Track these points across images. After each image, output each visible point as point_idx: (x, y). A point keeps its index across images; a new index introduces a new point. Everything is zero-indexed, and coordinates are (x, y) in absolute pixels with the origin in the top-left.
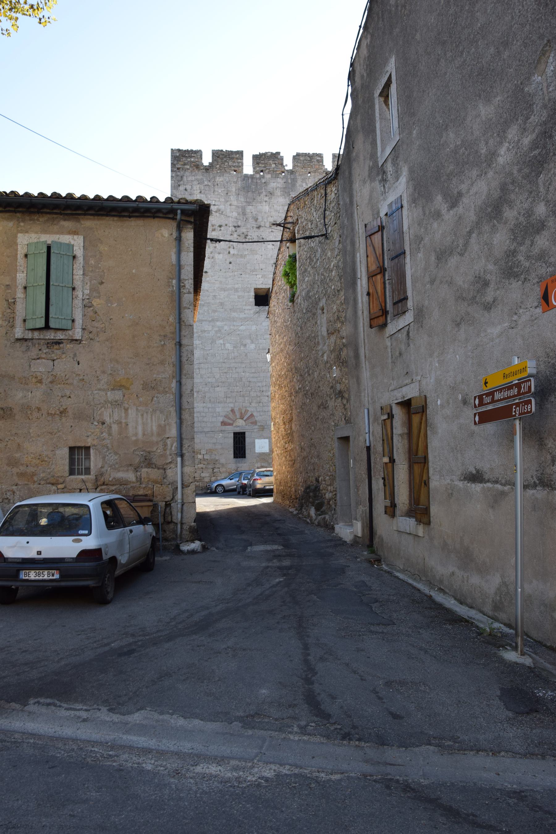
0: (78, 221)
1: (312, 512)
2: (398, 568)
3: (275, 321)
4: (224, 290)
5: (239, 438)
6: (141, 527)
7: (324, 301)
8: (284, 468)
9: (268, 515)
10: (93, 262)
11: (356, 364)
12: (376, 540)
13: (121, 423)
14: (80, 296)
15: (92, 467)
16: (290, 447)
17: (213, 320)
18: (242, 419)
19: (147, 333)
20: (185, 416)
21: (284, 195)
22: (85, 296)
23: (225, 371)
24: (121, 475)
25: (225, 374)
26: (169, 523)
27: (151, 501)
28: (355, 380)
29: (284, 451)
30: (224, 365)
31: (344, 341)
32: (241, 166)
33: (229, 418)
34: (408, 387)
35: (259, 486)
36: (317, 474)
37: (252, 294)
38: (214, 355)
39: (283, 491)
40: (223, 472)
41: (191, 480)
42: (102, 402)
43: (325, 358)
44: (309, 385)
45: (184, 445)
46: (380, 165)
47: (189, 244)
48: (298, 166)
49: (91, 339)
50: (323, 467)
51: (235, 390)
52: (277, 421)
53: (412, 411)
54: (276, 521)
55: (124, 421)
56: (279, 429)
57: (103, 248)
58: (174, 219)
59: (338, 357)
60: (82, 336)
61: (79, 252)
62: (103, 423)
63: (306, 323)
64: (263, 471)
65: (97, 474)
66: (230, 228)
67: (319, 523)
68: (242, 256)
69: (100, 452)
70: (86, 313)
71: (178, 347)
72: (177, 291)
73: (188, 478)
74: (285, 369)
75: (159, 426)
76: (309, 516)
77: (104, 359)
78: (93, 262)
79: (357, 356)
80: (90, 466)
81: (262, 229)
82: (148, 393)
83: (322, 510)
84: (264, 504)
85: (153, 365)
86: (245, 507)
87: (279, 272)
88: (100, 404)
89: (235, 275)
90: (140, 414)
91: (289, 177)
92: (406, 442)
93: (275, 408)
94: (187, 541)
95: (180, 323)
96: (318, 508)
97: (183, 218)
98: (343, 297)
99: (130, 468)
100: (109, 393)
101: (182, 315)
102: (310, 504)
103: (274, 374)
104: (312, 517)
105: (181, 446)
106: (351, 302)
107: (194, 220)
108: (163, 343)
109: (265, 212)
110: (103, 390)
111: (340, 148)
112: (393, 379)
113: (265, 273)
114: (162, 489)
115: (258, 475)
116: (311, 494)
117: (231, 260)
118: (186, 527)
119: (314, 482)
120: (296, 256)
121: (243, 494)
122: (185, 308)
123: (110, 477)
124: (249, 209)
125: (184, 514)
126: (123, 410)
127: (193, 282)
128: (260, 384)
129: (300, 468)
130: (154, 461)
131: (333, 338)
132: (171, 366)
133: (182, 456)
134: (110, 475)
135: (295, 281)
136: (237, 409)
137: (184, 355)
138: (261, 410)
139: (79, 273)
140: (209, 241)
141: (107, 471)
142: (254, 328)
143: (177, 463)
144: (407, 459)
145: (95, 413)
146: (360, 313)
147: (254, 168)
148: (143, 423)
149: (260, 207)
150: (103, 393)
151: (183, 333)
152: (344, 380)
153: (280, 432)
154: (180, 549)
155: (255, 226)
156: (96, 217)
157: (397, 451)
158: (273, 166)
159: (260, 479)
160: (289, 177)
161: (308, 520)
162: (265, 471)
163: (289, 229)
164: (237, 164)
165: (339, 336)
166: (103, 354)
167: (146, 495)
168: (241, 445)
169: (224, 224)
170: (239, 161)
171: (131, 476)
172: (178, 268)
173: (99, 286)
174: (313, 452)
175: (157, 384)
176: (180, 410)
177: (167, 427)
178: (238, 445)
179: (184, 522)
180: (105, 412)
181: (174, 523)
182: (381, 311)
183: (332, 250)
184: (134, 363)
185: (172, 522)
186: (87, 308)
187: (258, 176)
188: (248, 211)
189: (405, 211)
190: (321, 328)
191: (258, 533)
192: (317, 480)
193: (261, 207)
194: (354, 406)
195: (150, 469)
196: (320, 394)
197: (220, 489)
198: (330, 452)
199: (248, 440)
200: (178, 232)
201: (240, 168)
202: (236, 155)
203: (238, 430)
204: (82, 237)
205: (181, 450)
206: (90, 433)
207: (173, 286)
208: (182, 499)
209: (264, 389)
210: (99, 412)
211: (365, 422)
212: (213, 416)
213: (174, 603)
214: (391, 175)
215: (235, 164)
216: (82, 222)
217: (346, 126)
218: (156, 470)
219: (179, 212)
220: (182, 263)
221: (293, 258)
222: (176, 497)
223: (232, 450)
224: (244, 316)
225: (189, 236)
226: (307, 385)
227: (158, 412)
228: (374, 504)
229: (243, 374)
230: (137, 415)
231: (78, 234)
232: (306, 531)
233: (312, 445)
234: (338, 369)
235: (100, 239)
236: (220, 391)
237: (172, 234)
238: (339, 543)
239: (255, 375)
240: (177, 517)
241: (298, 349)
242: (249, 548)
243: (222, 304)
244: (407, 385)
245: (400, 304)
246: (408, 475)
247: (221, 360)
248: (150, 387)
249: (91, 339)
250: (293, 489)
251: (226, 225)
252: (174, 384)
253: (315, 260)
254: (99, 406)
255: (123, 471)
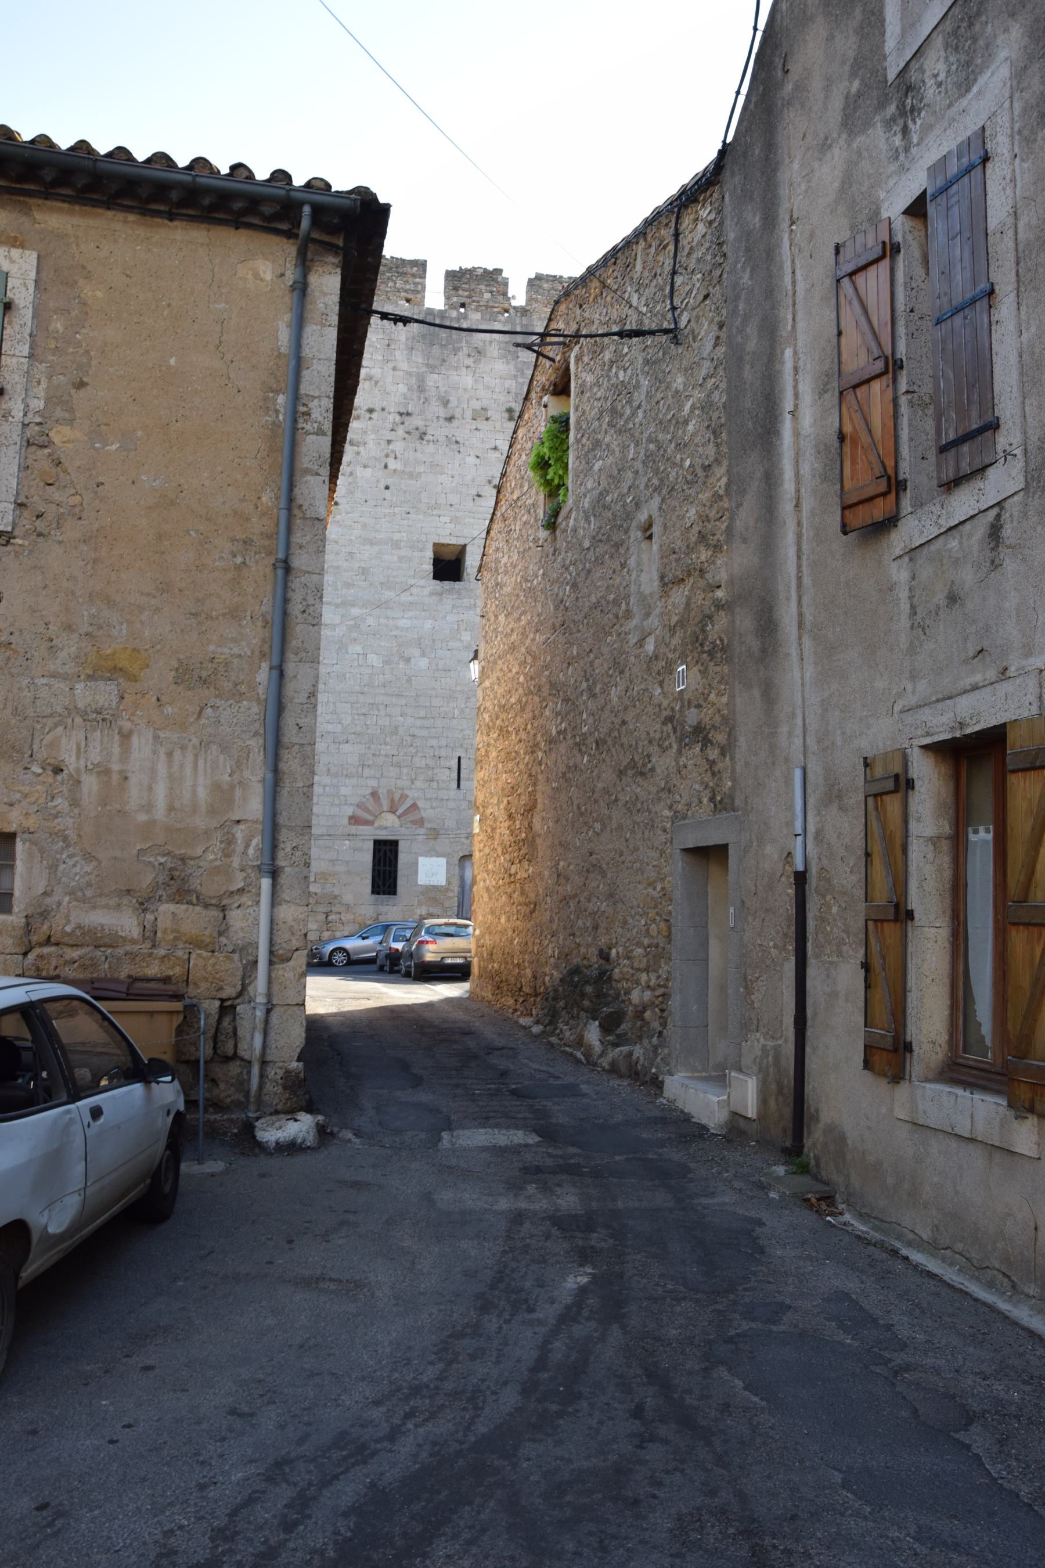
0: (26, 211)
1: (593, 1034)
2: (911, 1236)
3: (497, 584)
4: (372, 543)
5: (385, 852)
6: (137, 1088)
7: (656, 501)
8: (503, 920)
9: (467, 1032)
10: (59, 326)
11: (764, 651)
12: (815, 1139)
13: (107, 772)
14: (18, 414)
15: (17, 893)
16: (522, 872)
17: (344, 604)
18: (394, 813)
19: (197, 531)
20: (290, 763)
21: (505, 357)
22: (30, 415)
23: (363, 711)
24: (99, 918)
25: (362, 717)
26: (227, 1059)
27: (178, 997)
28: (756, 692)
29: (507, 880)
30: (361, 698)
31: (720, 594)
32: (420, 290)
33: (367, 810)
34: (985, 693)
35: (429, 957)
36: (603, 941)
37: (429, 554)
38: (342, 677)
39: (498, 973)
40: (349, 922)
41: (295, 943)
42: (59, 710)
43: (650, 647)
44: (591, 720)
45: (282, 845)
46: (891, 75)
47: (326, 306)
48: (537, 300)
49: (40, 535)
50: (625, 922)
51: (383, 752)
52: (488, 812)
53: (1011, 763)
54: (491, 1049)
55: (115, 767)
56: (494, 829)
57: (93, 292)
58: (290, 235)
59: (698, 640)
60: (14, 525)
61: (22, 294)
62: (58, 770)
63: (589, 572)
64: (440, 925)
65: (29, 912)
66: (391, 417)
67: (613, 1064)
68: (411, 476)
69: (42, 851)
70: (29, 462)
71: (280, 572)
72: (287, 426)
73: (287, 936)
74: (521, 691)
75: (216, 787)
76: (580, 1042)
77: (73, 593)
78: (59, 326)
79: (767, 625)
80: (13, 889)
81: (455, 423)
82: (189, 693)
83: (619, 1031)
84: (449, 1001)
85: (209, 617)
86: (407, 1006)
87: (514, 470)
88: (51, 716)
89: (394, 514)
90: (162, 751)
91: (518, 321)
92: (946, 860)
93: (485, 782)
94: (277, 1112)
95: (289, 509)
96: (610, 1025)
97: (316, 235)
98: (724, 480)
99: (125, 900)
100: (79, 687)
101: (296, 491)
102: (583, 1015)
103: (488, 704)
104: (590, 1047)
105: (274, 846)
106: (755, 487)
107: (345, 244)
108: (239, 560)
109: (465, 390)
110: (65, 677)
111: (738, 93)
112: (913, 677)
113: (458, 514)
114: (214, 965)
115: (428, 932)
116: (589, 989)
117: (389, 482)
118: (274, 1073)
119: (595, 959)
120: (568, 419)
121: (392, 972)
122: (307, 471)
123: (68, 922)
124: (432, 380)
125: (272, 1035)
126: (117, 737)
127: (331, 406)
128: (434, 742)
129: (551, 921)
130: (195, 884)
131: (678, 596)
132: (260, 624)
133: (274, 874)
134: (67, 917)
135: (561, 477)
136: (385, 791)
137: (296, 597)
138: (434, 796)
139: (17, 348)
140: (375, 320)
141: (59, 904)
142: (428, 624)
143: (259, 895)
144: (949, 912)
145: (37, 741)
146: (786, 507)
147: (448, 298)
148: (171, 777)
149: (454, 378)
150: (63, 686)
151: (297, 538)
152: (712, 696)
153: (497, 836)
154: (254, 1137)
155: (443, 415)
156: (77, 208)
157: (920, 887)
158: (487, 296)
159: (434, 942)
160: (518, 321)
161: (579, 1055)
162: (446, 924)
163: (553, 360)
164: (412, 287)
165: (702, 583)
166: (72, 578)
167: (166, 980)
168: (388, 868)
169: (378, 407)
170: (418, 280)
171: (126, 923)
172: (293, 363)
173: (73, 391)
174: (594, 884)
175: (215, 671)
176: (276, 747)
177: (238, 793)
178: (382, 868)
179: (269, 1058)
180: (64, 740)
181: (242, 1059)
182: (884, 482)
183: (688, 370)
184: (158, 610)
185: (235, 1056)
186: (34, 448)
187: (454, 314)
188: (430, 383)
189: (996, 173)
190: (638, 576)
191: (457, 1086)
192: (604, 956)
193: (457, 378)
194: (747, 764)
195: (184, 907)
196: (624, 740)
197: (339, 958)
198: (651, 884)
199: (403, 858)
200: (299, 270)
201: (419, 296)
202: (411, 268)
203: (383, 835)
204: (35, 255)
205: (273, 858)
206: (18, 796)
207: (277, 411)
208: (269, 995)
209: (443, 753)
210: (48, 738)
211: (792, 800)
212: (332, 804)
213: (233, 1412)
214: (940, 85)
215: (408, 287)
216: (38, 216)
217: (762, 25)
218: (198, 909)
219: (307, 209)
220: (306, 352)
221: (562, 424)
222: (250, 989)
223: (369, 876)
224: (411, 599)
225: (328, 284)
226: (582, 721)
227: (214, 748)
228: (809, 1033)
229: (401, 719)
230: (154, 752)
231: (22, 246)
232: (584, 1087)
233: (593, 868)
234: (696, 669)
235: (83, 267)
236: (351, 753)
237: (282, 275)
238: (687, 1130)
239: (426, 723)
240: (252, 1044)
241: (562, 639)
242: (445, 1135)
243: (364, 571)
244: (975, 688)
245: (965, 448)
246: (947, 958)
247: (357, 688)
248: (197, 677)
249: (40, 535)
250: (528, 972)
251: (383, 409)
252: (263, 675)
253: (628, 412)
254: (50, 722)
255: (106, 906)
